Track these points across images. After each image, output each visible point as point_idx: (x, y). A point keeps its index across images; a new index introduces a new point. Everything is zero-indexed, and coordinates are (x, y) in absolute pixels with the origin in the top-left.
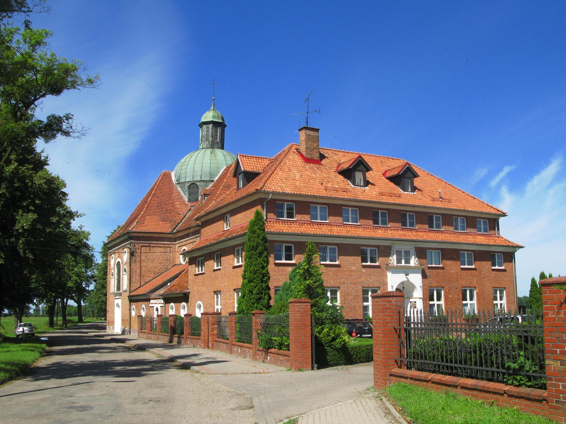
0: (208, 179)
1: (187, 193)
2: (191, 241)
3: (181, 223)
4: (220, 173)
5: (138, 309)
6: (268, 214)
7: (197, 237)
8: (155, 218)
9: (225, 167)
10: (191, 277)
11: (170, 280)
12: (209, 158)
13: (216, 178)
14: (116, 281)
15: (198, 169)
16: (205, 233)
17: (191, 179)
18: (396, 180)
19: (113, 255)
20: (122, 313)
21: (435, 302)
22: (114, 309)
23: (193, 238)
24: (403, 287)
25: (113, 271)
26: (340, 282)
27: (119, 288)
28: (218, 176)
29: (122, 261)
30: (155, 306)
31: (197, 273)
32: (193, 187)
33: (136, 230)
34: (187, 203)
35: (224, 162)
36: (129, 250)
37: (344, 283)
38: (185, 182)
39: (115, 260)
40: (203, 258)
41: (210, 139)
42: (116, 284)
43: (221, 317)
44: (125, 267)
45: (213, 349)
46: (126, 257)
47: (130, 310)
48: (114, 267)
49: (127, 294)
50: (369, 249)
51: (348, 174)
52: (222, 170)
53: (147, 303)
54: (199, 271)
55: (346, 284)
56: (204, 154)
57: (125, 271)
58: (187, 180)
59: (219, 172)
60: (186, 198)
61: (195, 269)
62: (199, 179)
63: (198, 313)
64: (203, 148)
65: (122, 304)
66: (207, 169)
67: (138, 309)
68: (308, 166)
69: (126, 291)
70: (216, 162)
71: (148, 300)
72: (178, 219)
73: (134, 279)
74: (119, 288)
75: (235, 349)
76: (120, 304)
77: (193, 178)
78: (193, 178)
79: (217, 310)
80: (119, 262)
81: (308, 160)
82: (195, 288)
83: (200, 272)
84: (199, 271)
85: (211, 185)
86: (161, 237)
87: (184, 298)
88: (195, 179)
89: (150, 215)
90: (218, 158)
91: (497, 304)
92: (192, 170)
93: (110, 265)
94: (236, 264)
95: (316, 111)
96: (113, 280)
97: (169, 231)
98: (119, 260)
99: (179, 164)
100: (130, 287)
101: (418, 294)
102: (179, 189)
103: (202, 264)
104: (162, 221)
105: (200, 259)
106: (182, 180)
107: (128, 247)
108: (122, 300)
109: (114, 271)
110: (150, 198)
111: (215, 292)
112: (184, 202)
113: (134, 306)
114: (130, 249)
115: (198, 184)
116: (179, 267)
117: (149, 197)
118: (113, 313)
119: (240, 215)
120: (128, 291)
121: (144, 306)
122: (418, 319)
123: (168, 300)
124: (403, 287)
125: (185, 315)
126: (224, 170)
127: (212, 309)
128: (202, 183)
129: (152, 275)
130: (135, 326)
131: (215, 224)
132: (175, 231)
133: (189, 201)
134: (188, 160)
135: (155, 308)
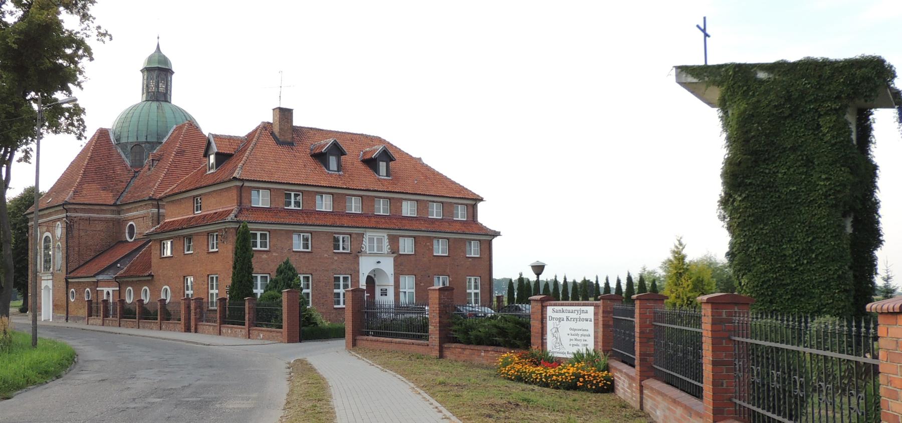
0: (155, 140)
6: (402, 278)
8: (94, 186)
9: (175, 127)
13: (165, 140)
29: (54, 236)
30: (106, 290)
33: (74, 201)
45: (196, 332)
46: (59, 231)
50: (341, 237)
58: (130, 140)
59: (167, 132)
65: (53, 286)
68: (280, 149)
72: (120, 187)
73: (71, 258)
76: (51, 287)
81: (279, 142)
87: (150, 280)
101: (389, 282)
102: (119, 150)
104: (103, 190)
106: (123, 140)
128: (148, 145)
129: (93, 254)
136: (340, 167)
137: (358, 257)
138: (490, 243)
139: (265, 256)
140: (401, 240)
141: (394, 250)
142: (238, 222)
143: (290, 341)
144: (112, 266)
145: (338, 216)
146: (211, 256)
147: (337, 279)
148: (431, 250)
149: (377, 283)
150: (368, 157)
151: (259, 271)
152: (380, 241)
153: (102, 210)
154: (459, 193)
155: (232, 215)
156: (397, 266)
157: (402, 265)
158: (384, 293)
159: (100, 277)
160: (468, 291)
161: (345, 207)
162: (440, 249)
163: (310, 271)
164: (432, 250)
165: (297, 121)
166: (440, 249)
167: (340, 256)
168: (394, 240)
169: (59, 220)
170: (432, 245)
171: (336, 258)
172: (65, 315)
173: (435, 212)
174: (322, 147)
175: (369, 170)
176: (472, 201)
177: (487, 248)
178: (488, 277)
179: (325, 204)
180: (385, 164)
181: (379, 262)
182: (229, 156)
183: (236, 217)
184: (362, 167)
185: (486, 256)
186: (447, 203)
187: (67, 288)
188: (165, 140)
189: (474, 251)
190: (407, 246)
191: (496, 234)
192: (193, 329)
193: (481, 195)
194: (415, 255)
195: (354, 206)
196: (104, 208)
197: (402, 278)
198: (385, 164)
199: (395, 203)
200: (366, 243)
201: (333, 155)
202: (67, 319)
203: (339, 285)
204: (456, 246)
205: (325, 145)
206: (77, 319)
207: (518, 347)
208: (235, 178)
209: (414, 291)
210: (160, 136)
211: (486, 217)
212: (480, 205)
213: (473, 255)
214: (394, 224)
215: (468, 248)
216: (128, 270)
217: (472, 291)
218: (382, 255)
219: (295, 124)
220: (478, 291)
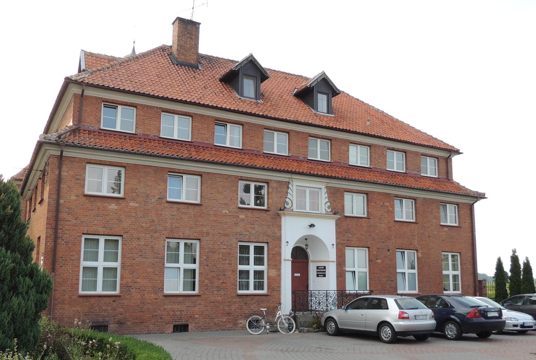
6: (348, 252)
37: (208, 234)
91: (448, 276)
124: (307, 245)
136: (259, 95)
137: (279, 216)
138: (471, 208)
139: (113, 206)
140: (347, 197)
141: (337, 209)
145: (249, 157)
147: (245, 249)
148: (392, 213)
149: (311, 258)
151: (101, 230)
152: (314, 195)
156: (339, 233)
157: (349, 232)
158: (322, 272)
160: (445, 272)
161: (262, 144)
162: (404, 212)
164: (393, 212)
165: (206, 47)
166: (404, 212)
167: (249, 214)
168: (336, 196)
170: (393, 206)
171: (242, 216)
173: (395, 163)
176: (446, 154)
177: (467, 213)
178: (470, 254)
179: (231, 137)
180: (325, 97)
181: (312, 226)
184: (295, 101)
185: (467, 224)
186: (411, 152)
189: (450, 217)
190: (355, 205)
191: (480, 196)
192: (318, 270)
193: (457, 146)
195: (278, 144)
197: (348, 252)
199: (339, 147)
201: (248, 76)
203: (248, 259)
204: (425, 210)
209: (367, 270)
211: (463, 173)
212: (455, 159)
213: (449, 224)
214: (338, 173)
215: (442, 214)
217: (450, 272)
219: (203, 50)
220: (458, 273)
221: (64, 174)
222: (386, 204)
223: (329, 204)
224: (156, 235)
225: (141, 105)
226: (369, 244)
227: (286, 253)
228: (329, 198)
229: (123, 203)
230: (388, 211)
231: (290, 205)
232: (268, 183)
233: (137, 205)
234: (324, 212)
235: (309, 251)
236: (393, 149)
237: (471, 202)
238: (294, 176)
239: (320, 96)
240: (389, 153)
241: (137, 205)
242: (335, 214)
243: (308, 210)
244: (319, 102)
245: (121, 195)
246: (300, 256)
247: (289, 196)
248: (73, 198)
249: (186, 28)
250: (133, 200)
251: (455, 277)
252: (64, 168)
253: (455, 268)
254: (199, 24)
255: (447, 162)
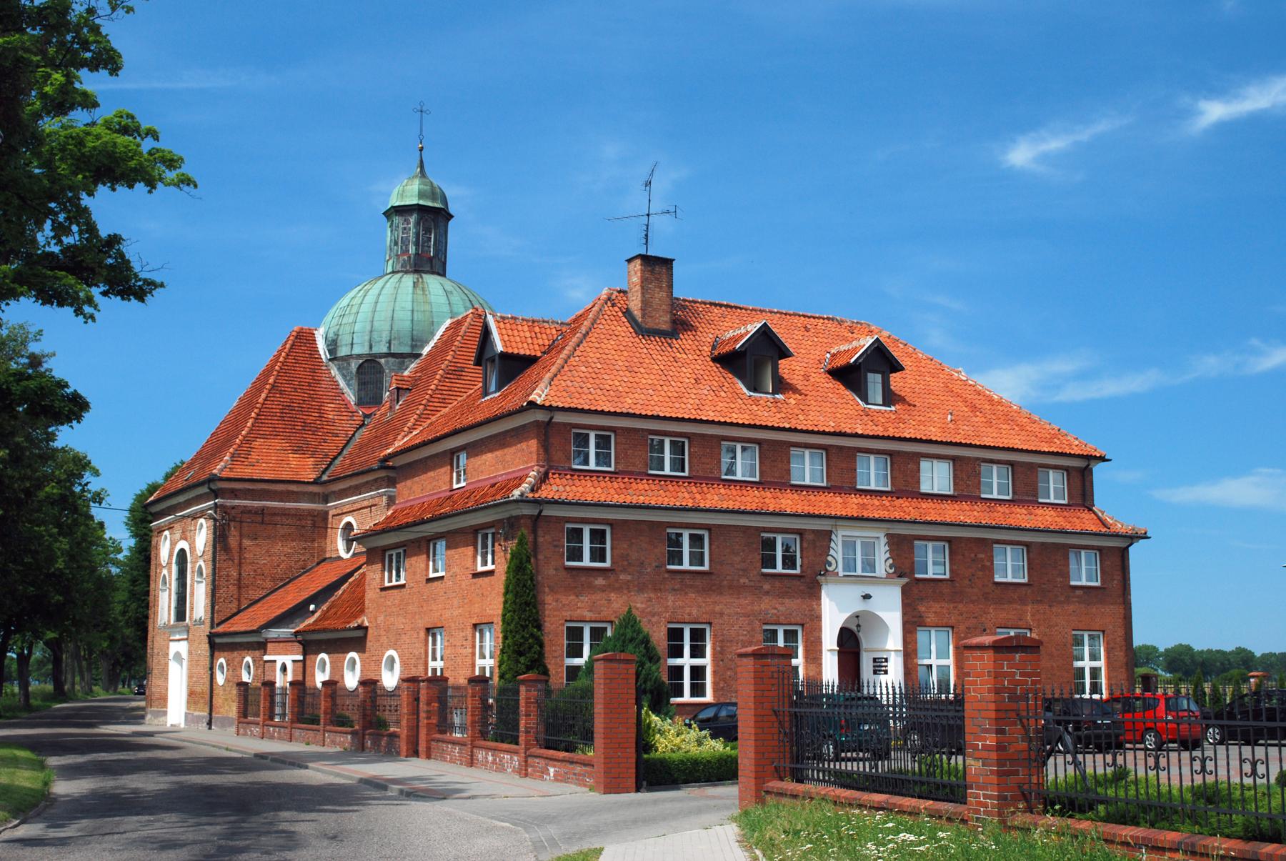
0: (406, 350)
1: (354, 382)
2: (366, 503)
3: (340, 458)
4: (437, 336)
5: (234, 667)
7: (380, 495)
8: (277, 444)
9: (448, 322)
10: (371, 595)
11: (318, 598)
12: (410, 297)
13: (426, 351)
14: (174, 597)
15: (383, 326)
16: (406, 492)
17: (365, 350)
18: (849, 376)
19: (167, 533)
20: (190, 677)
21: (686, 661)
22: (167, 665)
23: (372, 497)
24: (858, 626)
25: (165, 572)
26: (713, 612)
27: (181, 615)
28: (432, 344)
29: (193, 548)
30: (280, 659)
31: (387, 584)
32: (369, 371)
33: (232, 475)
34: (355, 408)
35: (446, 309)
36: (211, 523)
37: (722, 614)
38: (351, 356)
39: (173, 544)
40: (401, 550)
41: (412, 250)
42: (173, 605)
43: (446, 689)
44: (201, 563)
45: (429, 757)
46: (202, 536)
47: (212, 668)
48: (169, 563)
49: (206, 629)
51: (731, 361)
52: (442, 329)
53: (257, 653)
54: (390, 581)
55: (726, 617)
56: (396, 288)
57: (200, 573)
58: (357, 351)
59: (433, 334)
60: (351, 397)
61: (375, 576)
62: (384, 350)
63: (390, 680)
64: (393, 272)
65: (190, 653)
66: (404, 324)
67: (234, 667)
69: (201, 622)
70: (427, 308)
71: (262, 646)
72: (331, 446)
74: (181, 615)
75: (480, 755)
76: (185, 655)
77: (371, 347)
78: (371, 347)
79: (434, 670)
80: (182, 551)
81: (643, 331)
82: (381, 619)
83: (394, 583)
84: (390, 581)
85: (413, 366)
86: (293, 492)
87: (357, 640)
88: (375, 350)
89: (264, 437)
90: (433, 299)
91: (1083, 669)
92: (369, 328)
93: (157, 555)
94: (480, 569)
95: (668, 212)
96: (167, 593)
97: (312, 476)
98: (183, 544)
99: (334, 311)
100: (213, 613)
102: (334, 371)
103: (398, 562)
104: (295, 452)
105: (394, 553)
106: (343, 351)
107: (211, 517)
108: (190, 645)
109: (170, 572)
110: (263, 395)
111: (428, 630)
112: (347, 405)
113: (222, 660)
114: (215, 520)
115: (383, 361)
116: (335, 564)
117: (260, 391)
118: (164, 674)
119: (489, 455)
120: (208, 621)
121: (248, 659)
122: (894, 698)
123: (310, 645)
124: (858, 626)
125: (324, 683)
126: (448, 329)
127: (421, 668)
128: (391, 360)
129: (269, 584)
130: (229, 708)
131: (431, 474)
132: (325, 478)
133: (360, 403)
134: (357, 301)
135: (278, 666)
138: (1123, 554)
142: (536, 502)
143: (612, 786)
144: (299, 610)
146: (480, 580)
149: (864, 644)
150: (840, 362)
151: (588, 615)
152: (869, 548)
153: (268, 491)
154: (1050, 442)
155: (525, 487)
158: (880, 666)
159: (274, 633)
160: (1078, 664)
161: (788, 472)
163: (706, 617)
169: (201, 514)
172: (206, 714)
174: (736, 341)
175: (849, 394)
180: (878, 377)
181: (867, 597)
182: (530, 361)
183: (532, 490)
187: (212, 656)
188: (426, 351)
192: (422, 748)
194: (951, 580)
196: (293, 488)
197: (639, 261)
198: (878, 377)
200: (837, 552)
202: (210, 724)
205: (742, 336)
206: (225, 722)
207: (500, 667)
208: (532, 405)
210: (418, 342)
215: (1073, 566)
216: (324, 617)
217: (1087, 664)
218: (875, 580)
220: (1101, 663)
221: (540, 539)
222: (981, 556)
223: (891, 561)
224: (654, 620)
225: (622, 428)
226: (953, 621)
227: (829, 640)
228: (891, 551)
229: (612, 577)
230: (984, 568)
231: (834, 566)
232: (689, 438)
233: (629, 577)
234: (883, 574)
235: (861, 635)
236: (992, 461)
237: (1124, 545)
238: (840, 522)
239: (871, 376)
240: (984, 466)
241: (629, 577)
242: (900, 576)
243: (859, 572)
244: (870, 386)
245: (607, 564)
246: (849, 642)
247: (832, 552)
248: (552, 572)
249: (652, 272)
250: (624, 571)
251: (1095, 672)
252: (540, 532)
253: (1094, 657)
254: (672, 260)
255: (1083, 476)
